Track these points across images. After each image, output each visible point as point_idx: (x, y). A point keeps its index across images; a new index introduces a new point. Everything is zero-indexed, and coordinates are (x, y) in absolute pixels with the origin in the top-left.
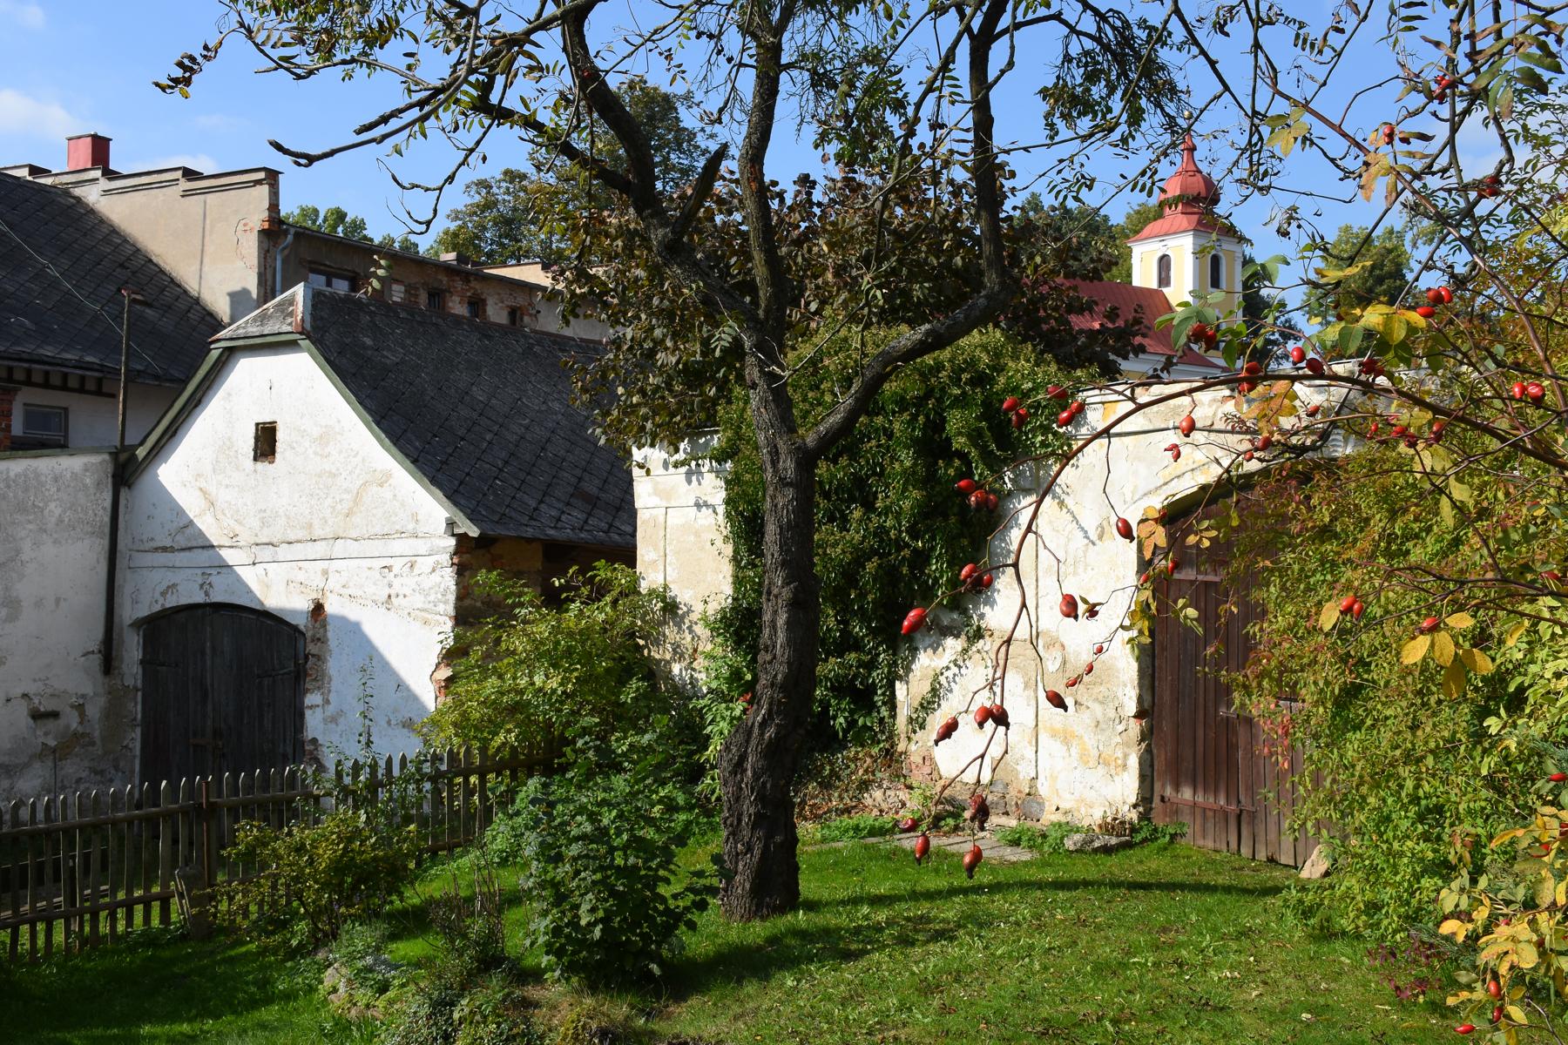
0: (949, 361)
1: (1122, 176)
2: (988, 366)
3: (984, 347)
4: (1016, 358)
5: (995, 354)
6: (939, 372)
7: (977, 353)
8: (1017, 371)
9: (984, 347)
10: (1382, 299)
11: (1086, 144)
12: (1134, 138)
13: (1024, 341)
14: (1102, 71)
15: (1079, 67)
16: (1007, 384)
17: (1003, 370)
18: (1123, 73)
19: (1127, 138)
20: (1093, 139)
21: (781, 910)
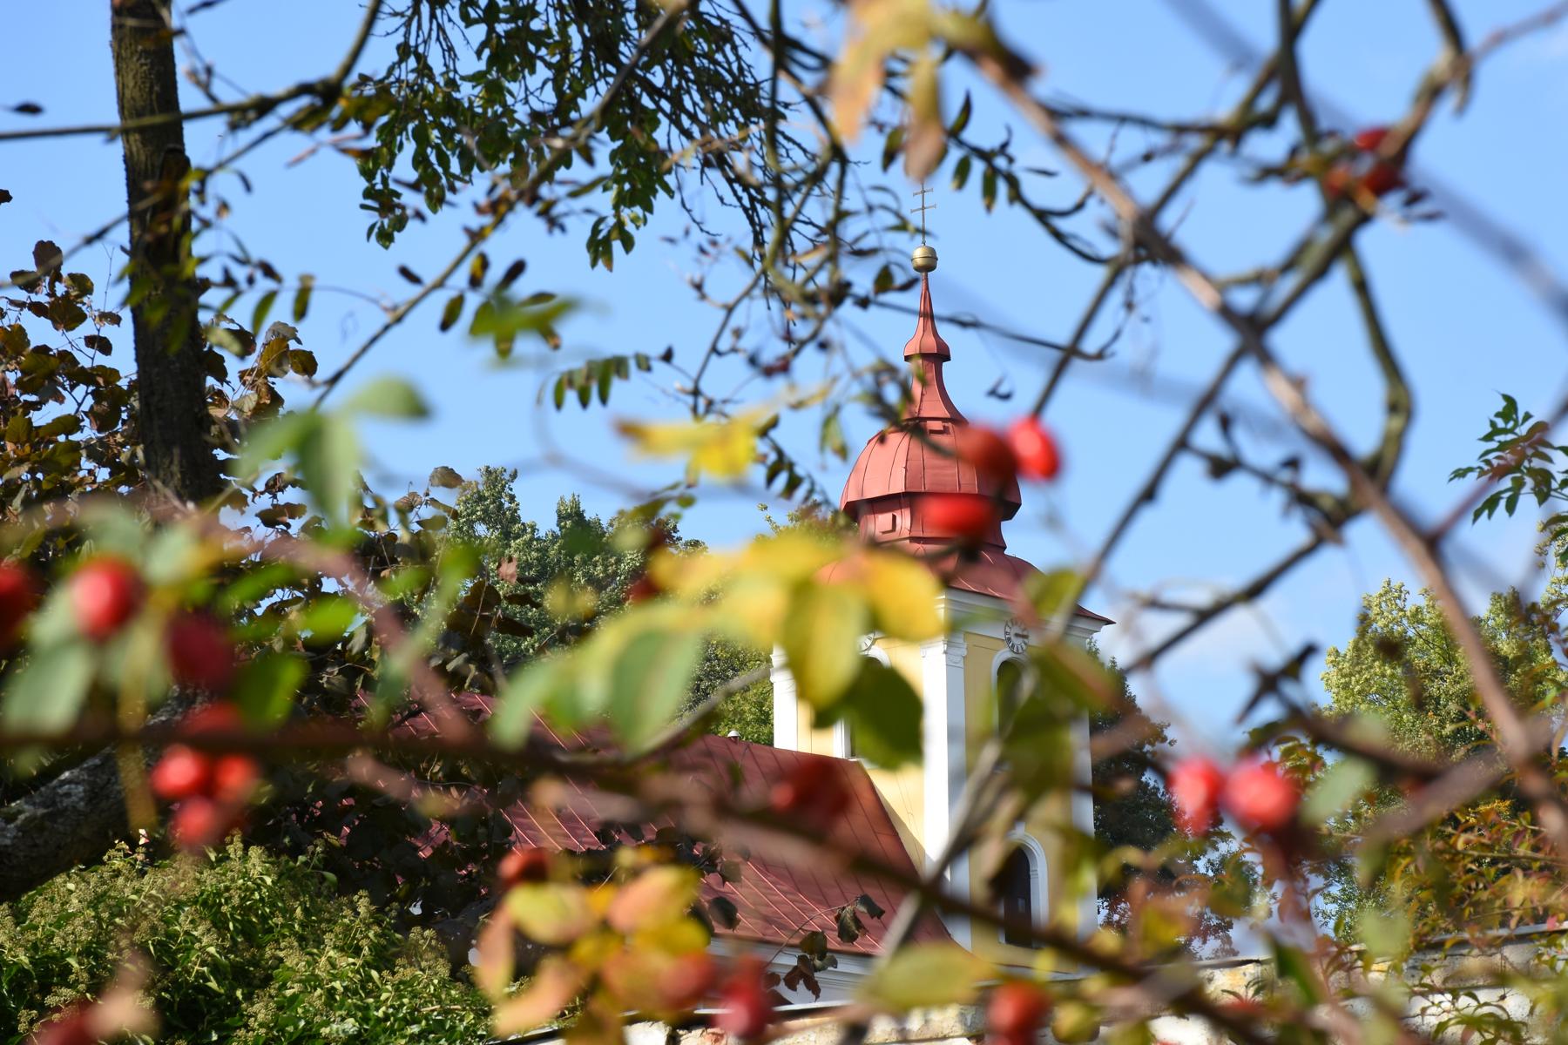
0: (87, 952)
1: (405, 273)
2: (216, 969)
3: (209, 906)
4: (309, 940)
5: (247, 931)
6: (46, 989)
7: (183, 925)
8: (312, 982)
9: (209, 906)
10: (586, 29)
11: (245, 137)
12: (628, 243)
13: (347, 887)
14: (541, 38)
15: (469, 22)
16: (277, 1025)
17: (267, 980)
18: (604, 45)
19: (607, 242)
20: (270, 122)
21: (1463, 692)
